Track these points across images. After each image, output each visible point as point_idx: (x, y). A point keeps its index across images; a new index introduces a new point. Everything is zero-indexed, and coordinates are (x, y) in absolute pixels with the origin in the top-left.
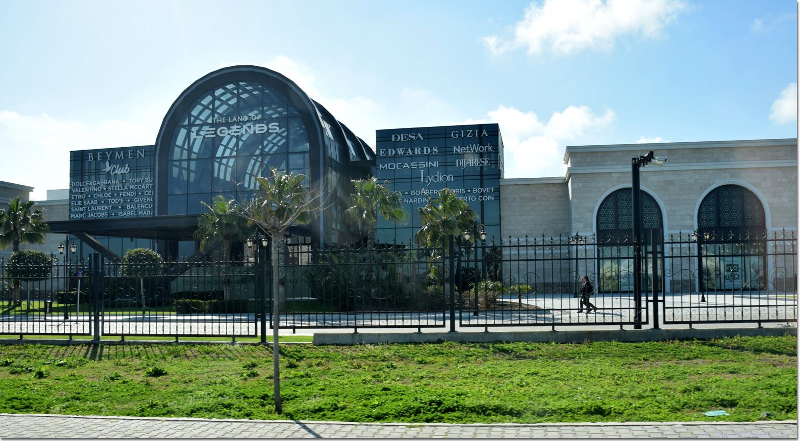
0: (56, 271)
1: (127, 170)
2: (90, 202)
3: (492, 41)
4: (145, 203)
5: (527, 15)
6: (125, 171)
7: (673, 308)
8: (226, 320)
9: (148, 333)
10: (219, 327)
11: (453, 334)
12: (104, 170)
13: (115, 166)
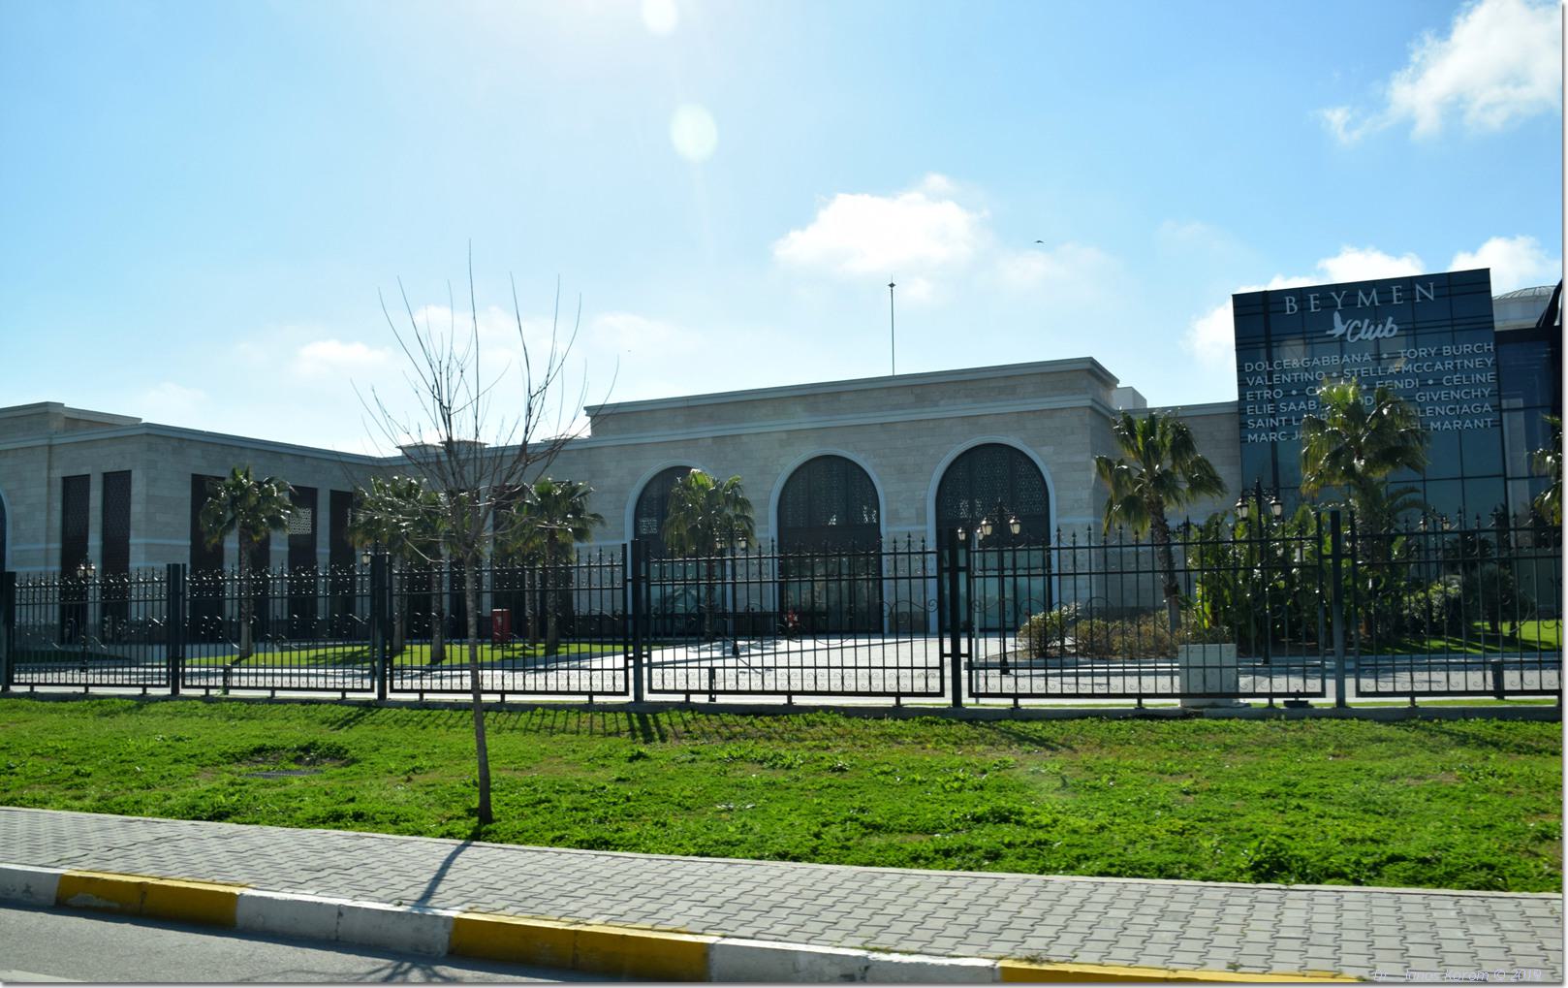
0: (682, 571)
1: (1391, 330)
2: (1297, 405)
3: (1337, 116)
4: (1446, 403)
5: (1415, 58)
6: (1386, 333)
7: (870, 668)
8: (1411, 664)
9: (760, 689)
10: (870, 677)
11: (956, 709)
12: (1328, 332)
13: (1357, 322)
